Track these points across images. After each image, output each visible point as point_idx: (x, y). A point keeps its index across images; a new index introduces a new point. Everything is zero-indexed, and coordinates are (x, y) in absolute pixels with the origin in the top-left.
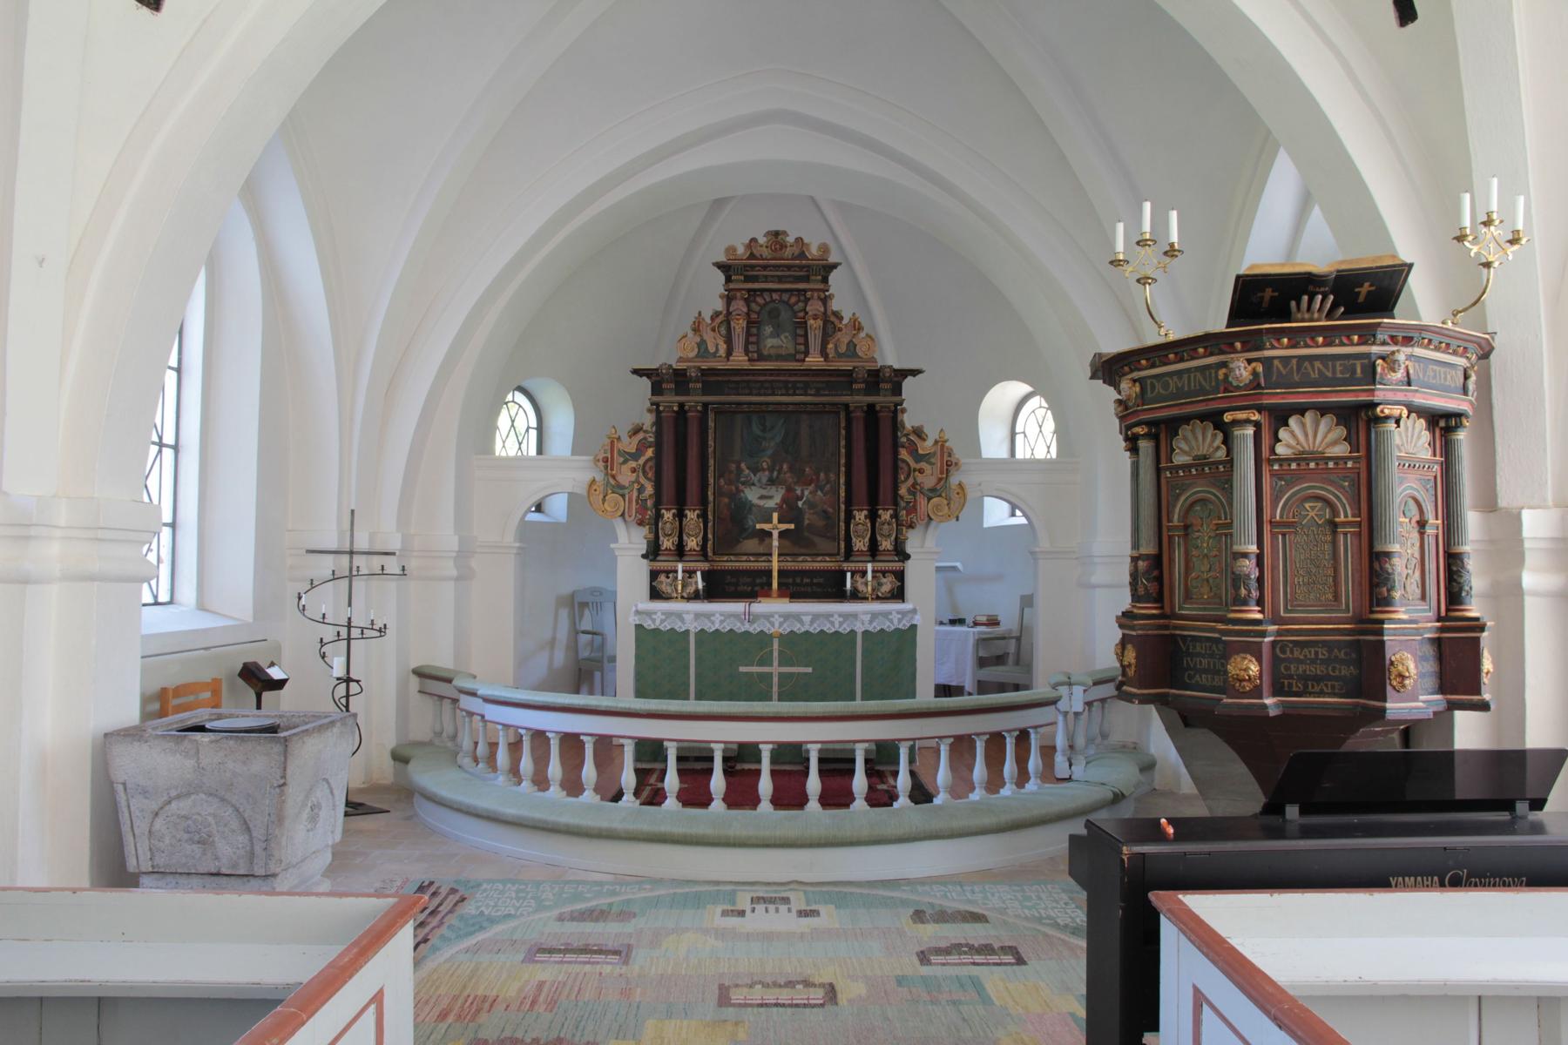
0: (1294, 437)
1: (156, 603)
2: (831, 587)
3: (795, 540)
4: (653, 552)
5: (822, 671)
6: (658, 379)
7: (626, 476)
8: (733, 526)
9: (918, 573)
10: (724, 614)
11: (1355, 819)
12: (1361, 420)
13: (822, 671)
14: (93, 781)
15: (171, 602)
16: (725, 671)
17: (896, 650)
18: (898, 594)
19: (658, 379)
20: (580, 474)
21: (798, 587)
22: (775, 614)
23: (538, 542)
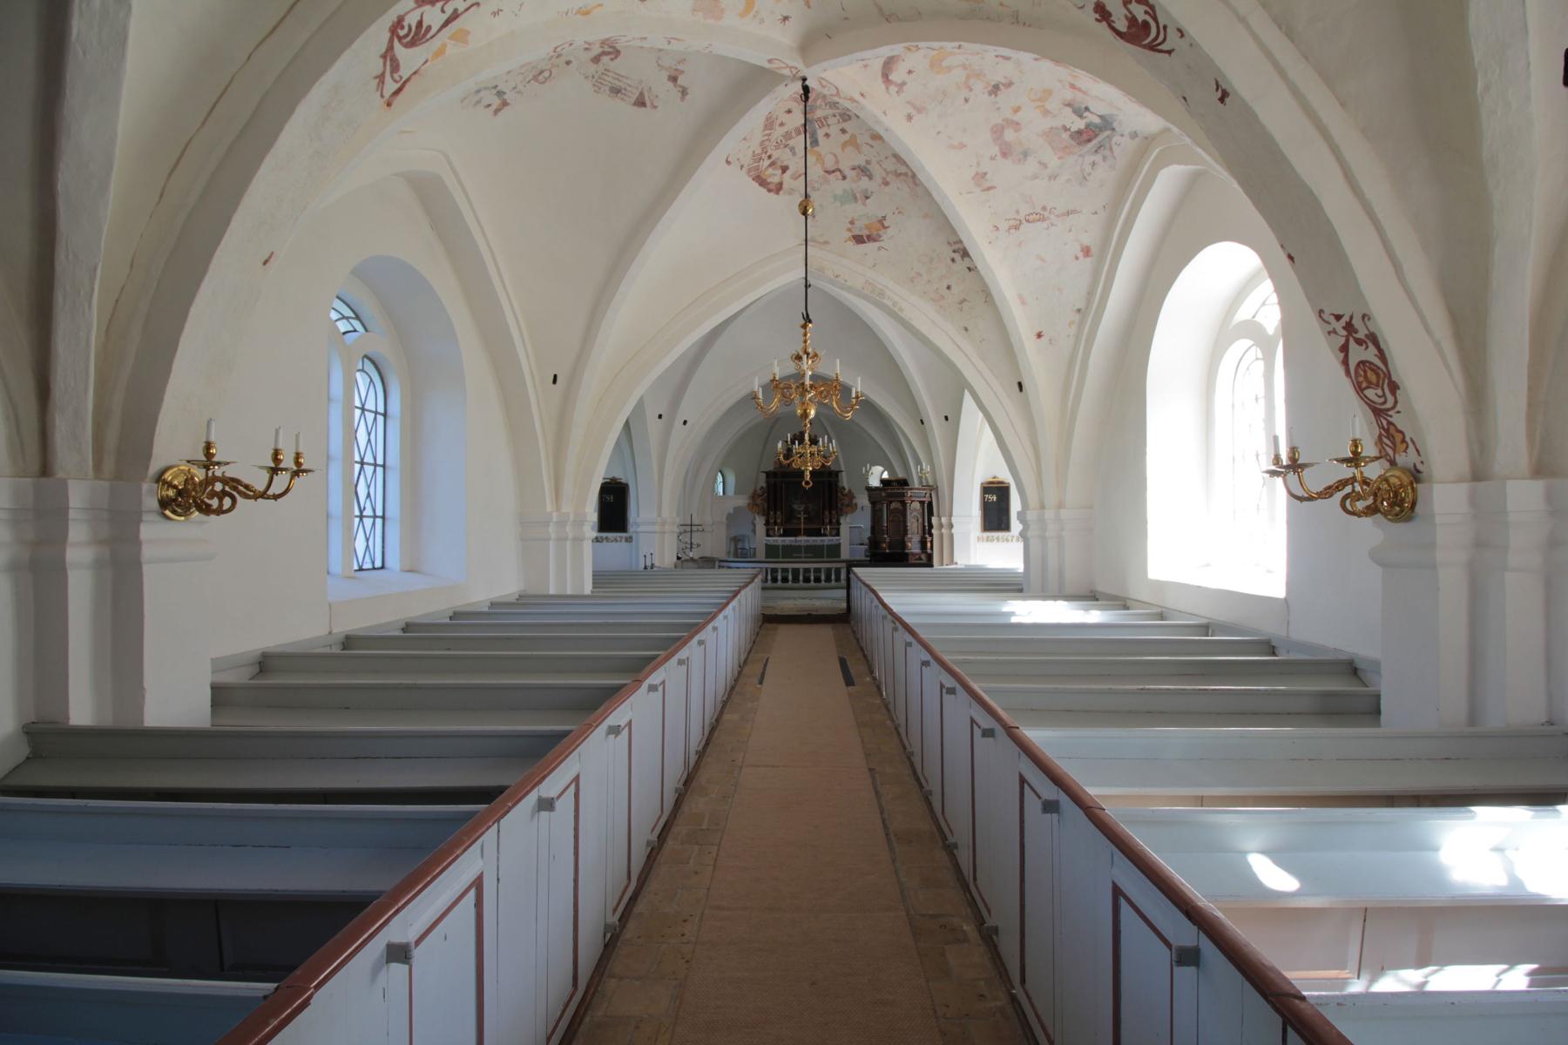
0: (893, 505)
1: (361, 569)
2: (818, 533)
3: (808, 520)
4: (767, 523)
5: (816, 552)
6: (768, 474)
7: (759, 501)
8: (790, 516)
9: (844, 529)
10: (789, 540)
11: (1074, 382)
12: (904, 504)
13: (816, 552)
14: (1144, 453)
15: (383, 567)
16: (789, 552)
17: (835, 550)
18: (838, 534)
19: (768, 474)
20: (742, 501)
21: (809, 533)
22: (803, 540)
23: (732, 518)
